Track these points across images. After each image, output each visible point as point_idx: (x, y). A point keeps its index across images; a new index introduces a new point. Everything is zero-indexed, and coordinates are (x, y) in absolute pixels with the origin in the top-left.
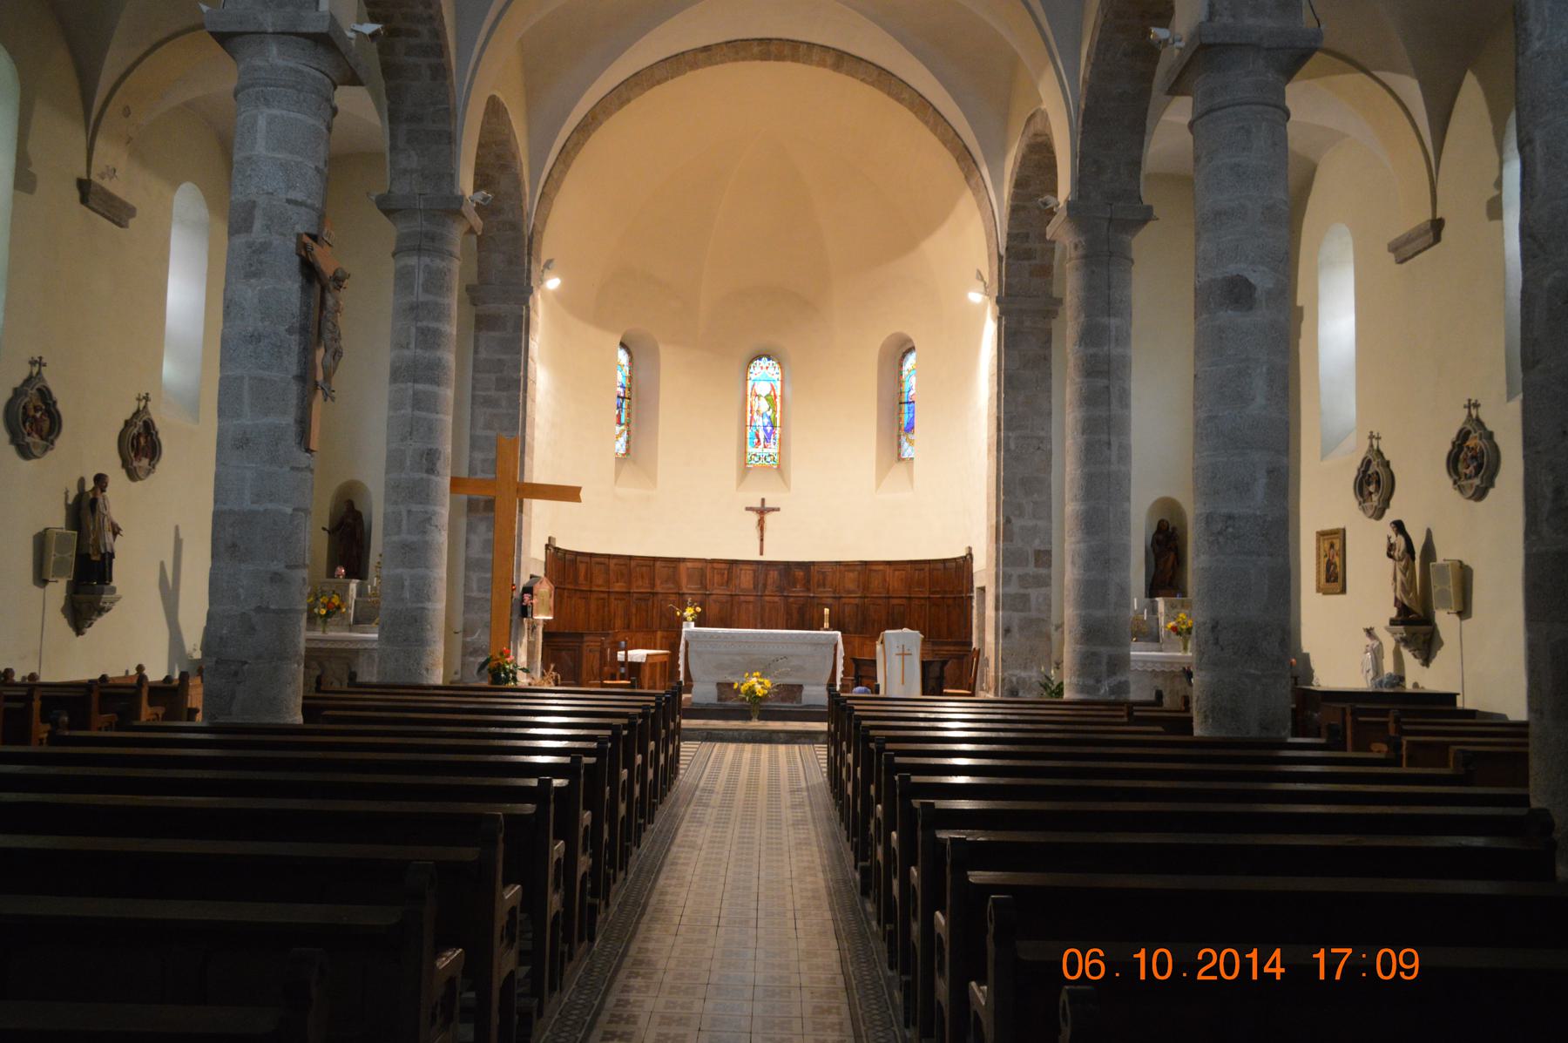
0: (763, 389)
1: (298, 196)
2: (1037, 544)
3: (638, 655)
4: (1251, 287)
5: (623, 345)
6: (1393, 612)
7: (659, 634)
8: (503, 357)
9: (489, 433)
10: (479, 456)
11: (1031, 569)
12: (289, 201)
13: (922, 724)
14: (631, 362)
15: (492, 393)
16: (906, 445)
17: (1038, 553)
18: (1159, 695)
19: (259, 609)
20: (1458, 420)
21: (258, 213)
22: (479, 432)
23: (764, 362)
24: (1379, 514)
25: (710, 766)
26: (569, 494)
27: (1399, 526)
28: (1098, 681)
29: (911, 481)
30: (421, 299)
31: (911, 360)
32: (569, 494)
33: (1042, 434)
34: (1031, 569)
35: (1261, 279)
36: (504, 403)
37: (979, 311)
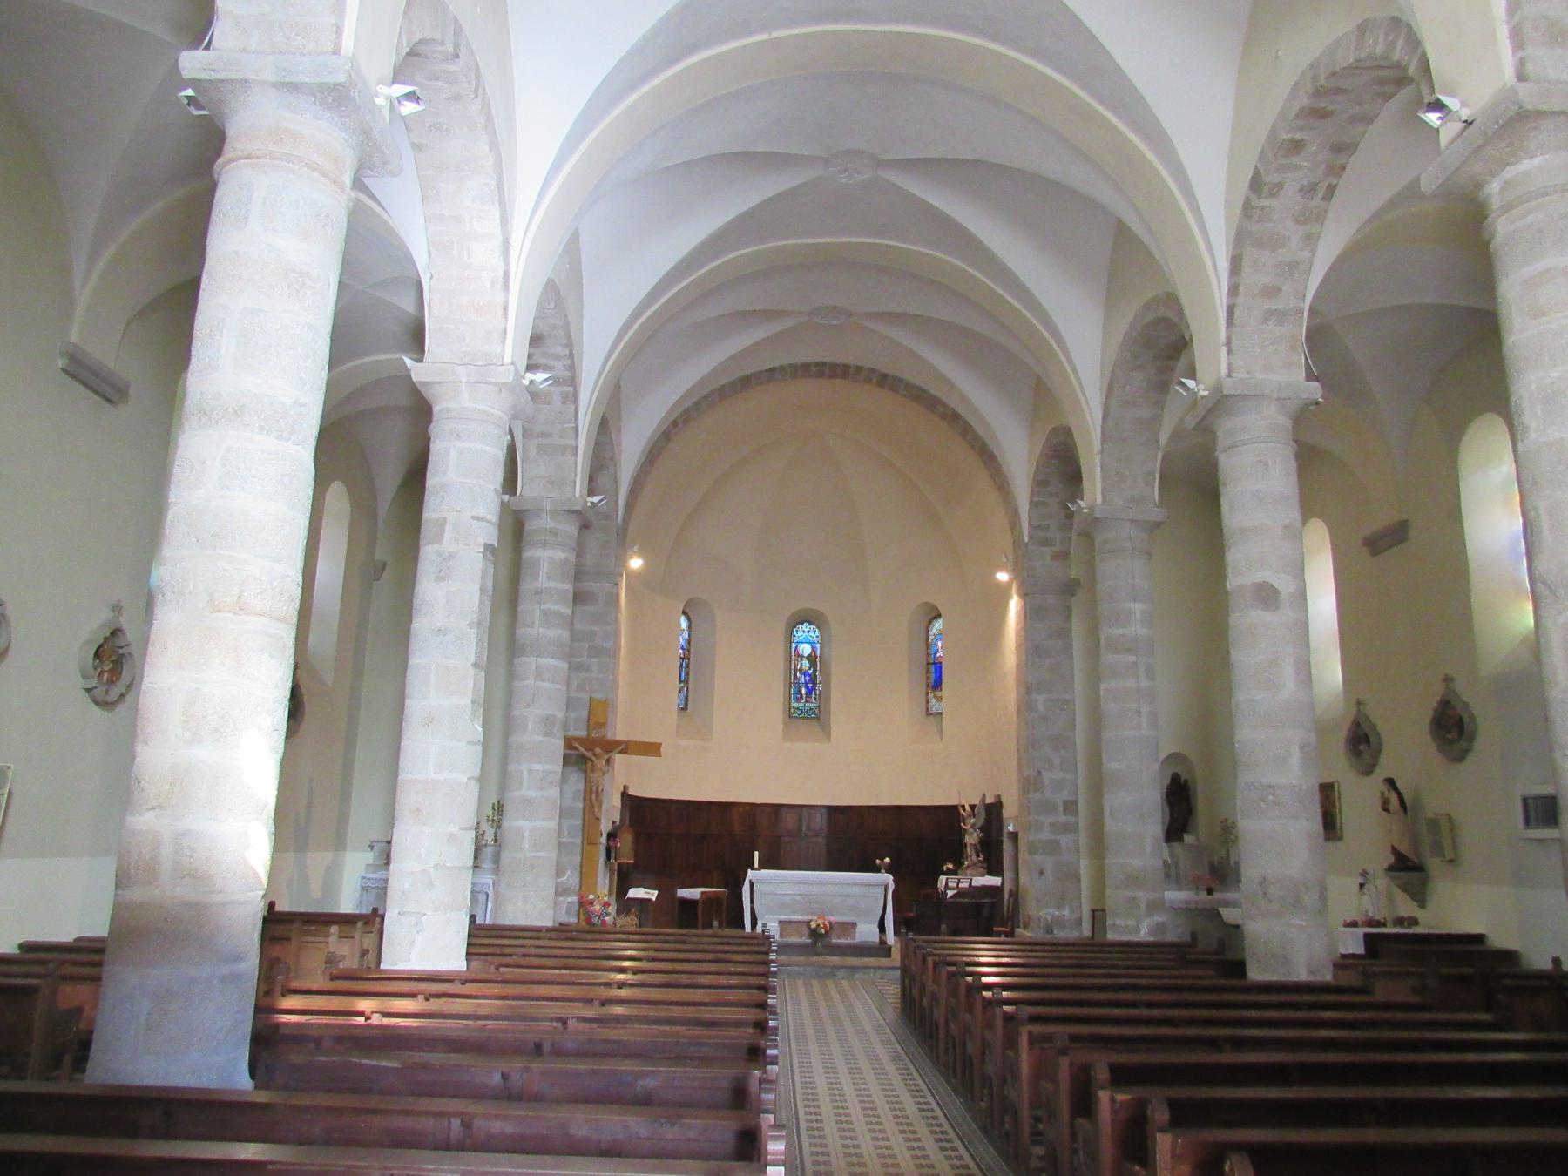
0: (806, 649)
1: (481, 513)
2: (1065, 795)
3: (694, 893)
4: (1275, 591)
5: (684, 613)
6: (1391, 859)
7: (715, 874)
8: (596, 628)
9: (581, 695)
10: (573, 715)
11: (1062, 818)
12: (474, 518)
13: (1165, 997)
14: (690, 627)
15: (584, 659)
16: (933, 701)
17: (1066, 803)
18: (1194, 936)
19: (436, 867)
20: (1436, 693)
21: (448, 528)
22: (573, 694)
23: (806, 627)
24: (1368, 770)
25: (796, 1005)
26: (652, 749)
27: (1391, 783)
28: (1139, 922)
29: (941, 732)
30: (546, 585)
31: (938, 625)
32: (652, 749)
33: (1067, 697)
34: (1062, 818)
35: (1284, 585)
36: (595, 669)
37: (1002, 594)
